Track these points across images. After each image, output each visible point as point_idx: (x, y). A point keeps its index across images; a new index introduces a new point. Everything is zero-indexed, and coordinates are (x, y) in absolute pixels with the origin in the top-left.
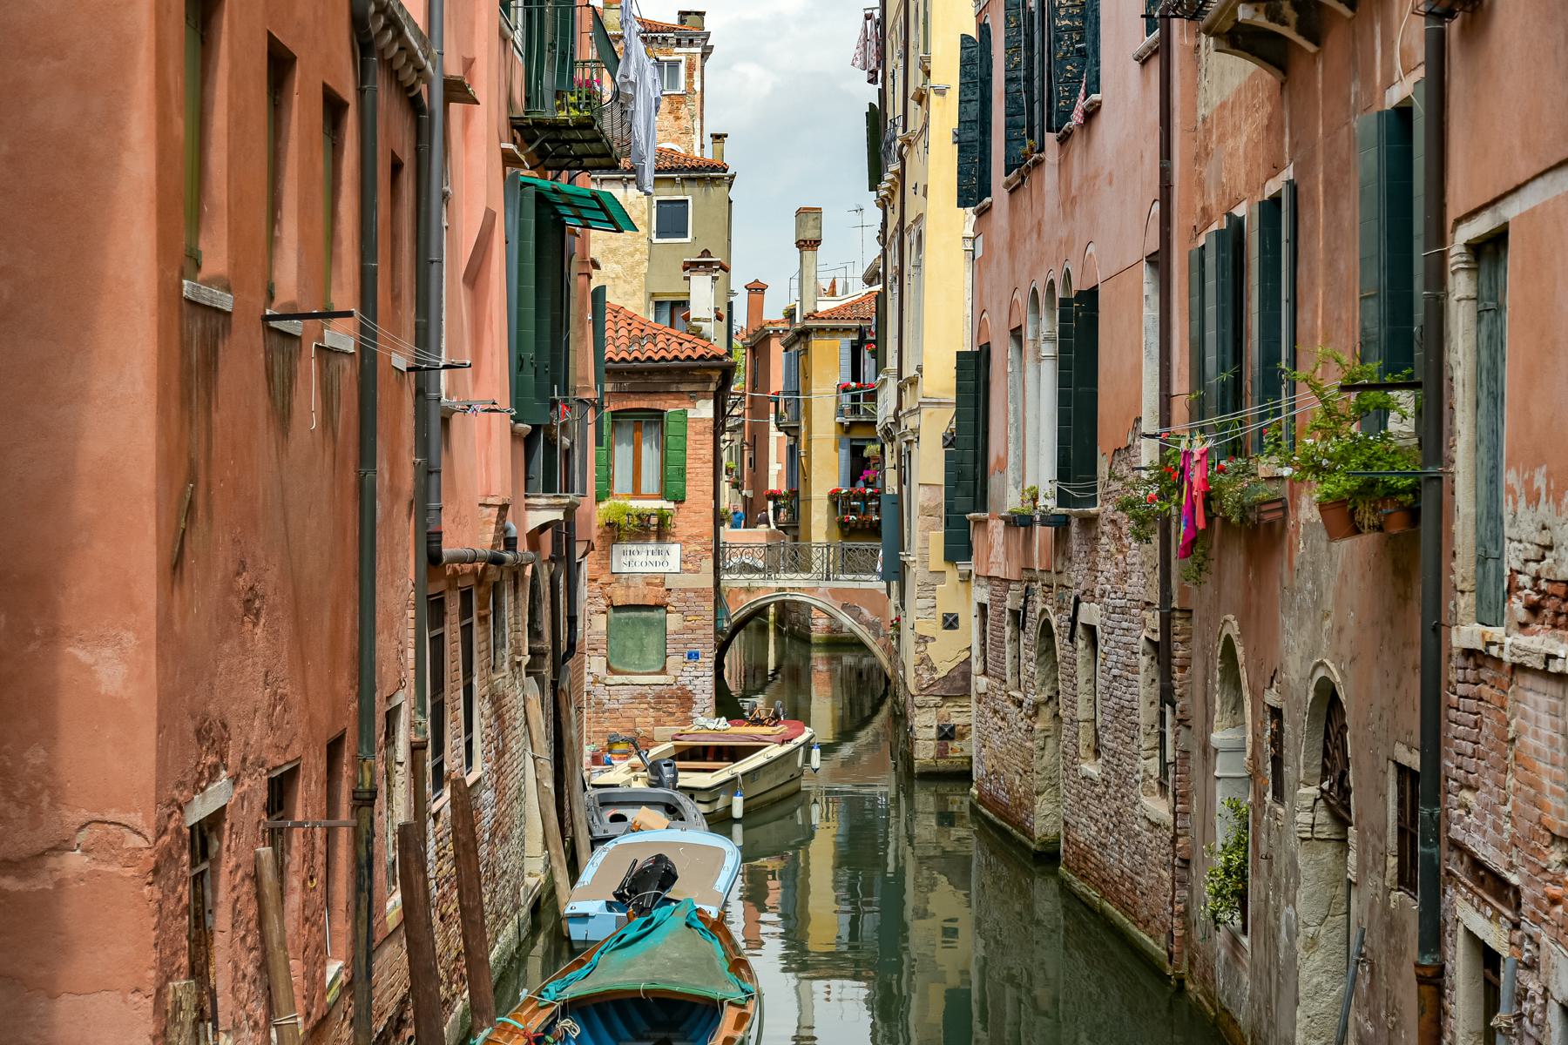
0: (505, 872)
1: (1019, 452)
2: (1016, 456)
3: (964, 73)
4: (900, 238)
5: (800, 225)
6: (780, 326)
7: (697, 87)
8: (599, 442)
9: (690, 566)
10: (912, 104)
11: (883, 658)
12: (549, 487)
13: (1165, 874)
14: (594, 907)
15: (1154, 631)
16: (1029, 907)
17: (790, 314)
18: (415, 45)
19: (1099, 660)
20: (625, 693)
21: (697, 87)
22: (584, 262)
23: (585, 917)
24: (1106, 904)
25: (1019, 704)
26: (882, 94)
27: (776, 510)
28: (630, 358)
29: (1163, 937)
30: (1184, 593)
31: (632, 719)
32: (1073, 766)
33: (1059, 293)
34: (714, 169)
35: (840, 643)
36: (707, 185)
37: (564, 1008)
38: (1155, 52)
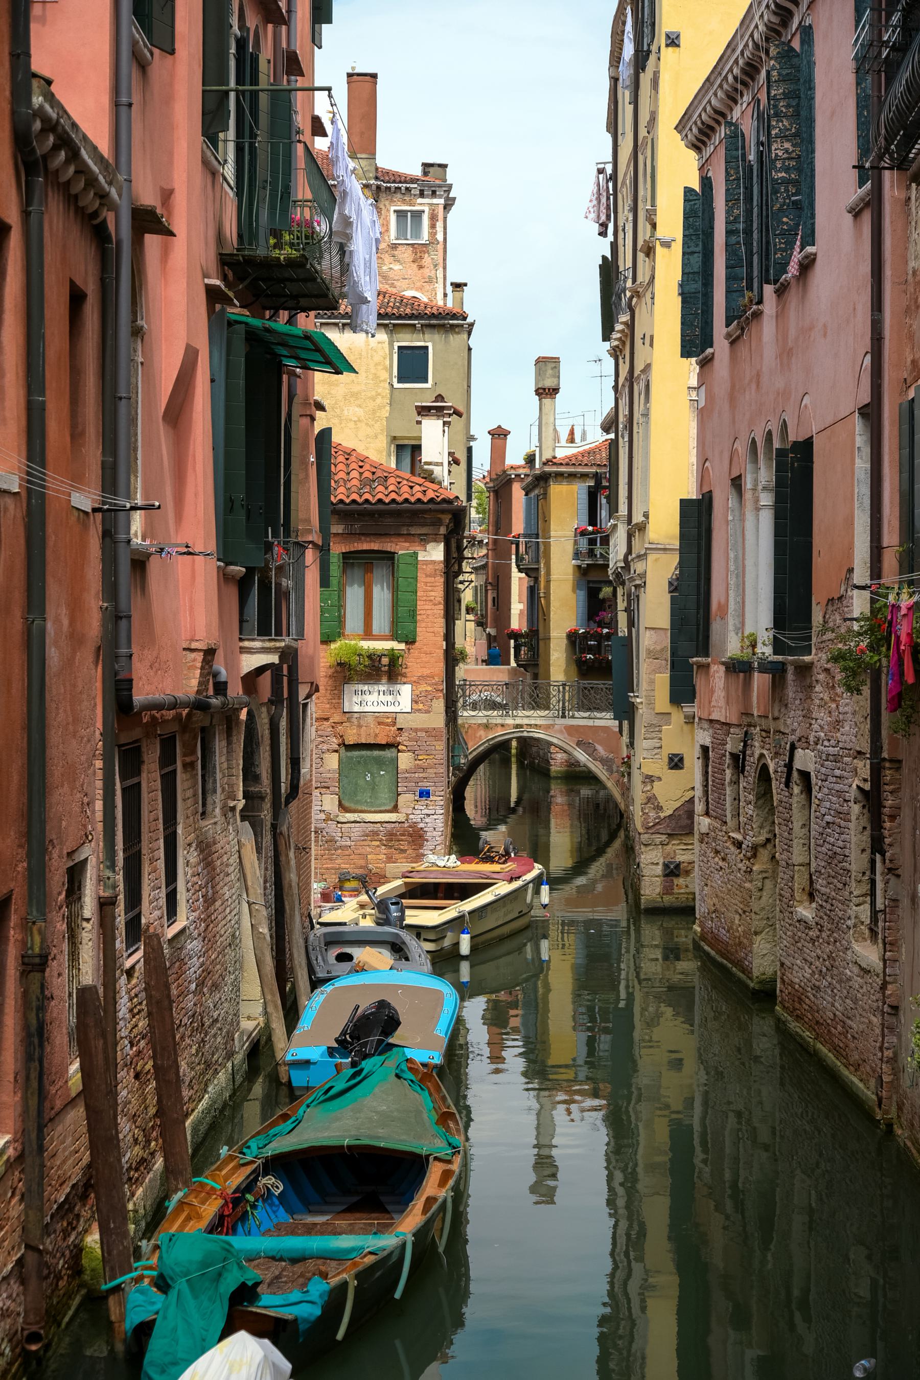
0: (216, 1021)
1: (739, 599)
2: (736, 603)
3: (686, 228)
4: (631, 384)
5: (539, 374)
6: (521, 471)
7: (440, 237)
8: (325, 582)
9: (421, 706)
10: (641, 256)
11: (617, 794)
12: (264, 631)
13: (875, 1020)
14: (315, 1053)
15: (865, 780)
16: (748, 1043)
17: (530, 459)
18: (95, 169)
19: (814, 806)
20: (357, 830)
21: (440, 237)
22: (306, 403)
23: (307, 1062)
24: (819, 1046)
25: (739, 845)
26: (614, 246)
27: (517, 649)
28: (360, 500)
29: (873, 1083)
30: (894, 743)
31: (364, 856)
32: (788, 908)
33: (777, 444)
34: (454, 316)
35: (577, 776)
36: (446, 332)
37: (266, 1165)
38: (867, 205)
